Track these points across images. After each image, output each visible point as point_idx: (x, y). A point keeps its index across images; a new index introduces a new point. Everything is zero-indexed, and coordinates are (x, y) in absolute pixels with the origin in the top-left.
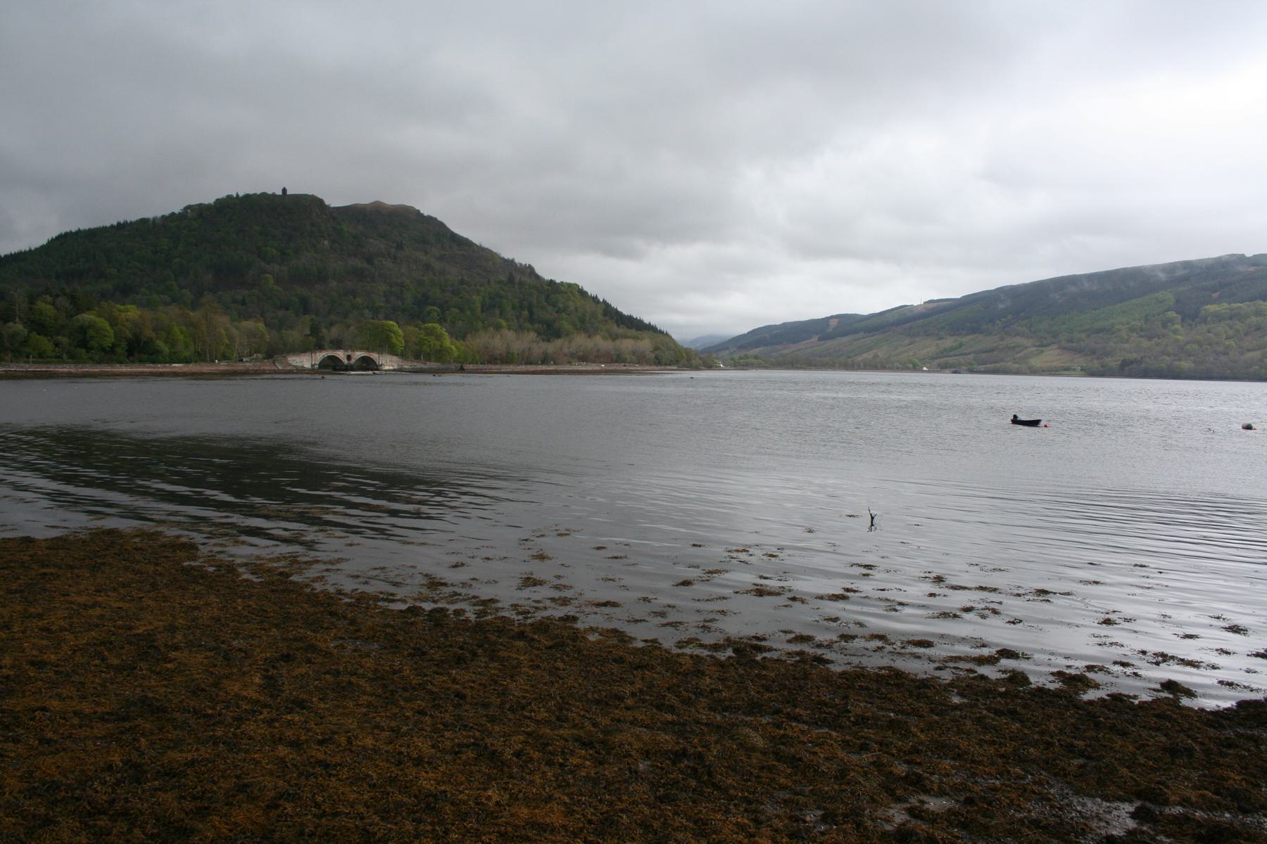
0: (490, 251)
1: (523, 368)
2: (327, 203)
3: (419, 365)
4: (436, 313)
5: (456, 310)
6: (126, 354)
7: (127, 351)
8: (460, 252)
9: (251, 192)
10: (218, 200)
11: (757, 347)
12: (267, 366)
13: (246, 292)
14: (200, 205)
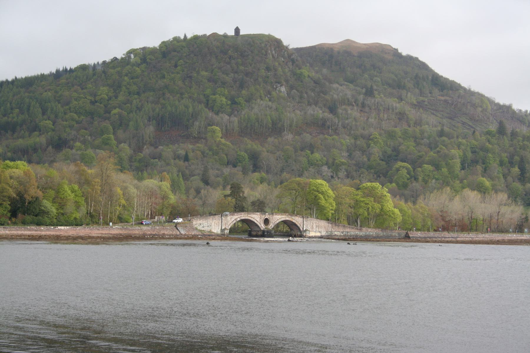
0: (482, 96)
1: (488, 236)
2: (285, 43)
3: (353, 232)
4: (405, 171)
5: (430, 167)
6: (9, 215)
7: (10, 211)
8: (443, 98)
10: (163, 43)
12: (168, 230)
13: (191, 147)
14: (144, 49)
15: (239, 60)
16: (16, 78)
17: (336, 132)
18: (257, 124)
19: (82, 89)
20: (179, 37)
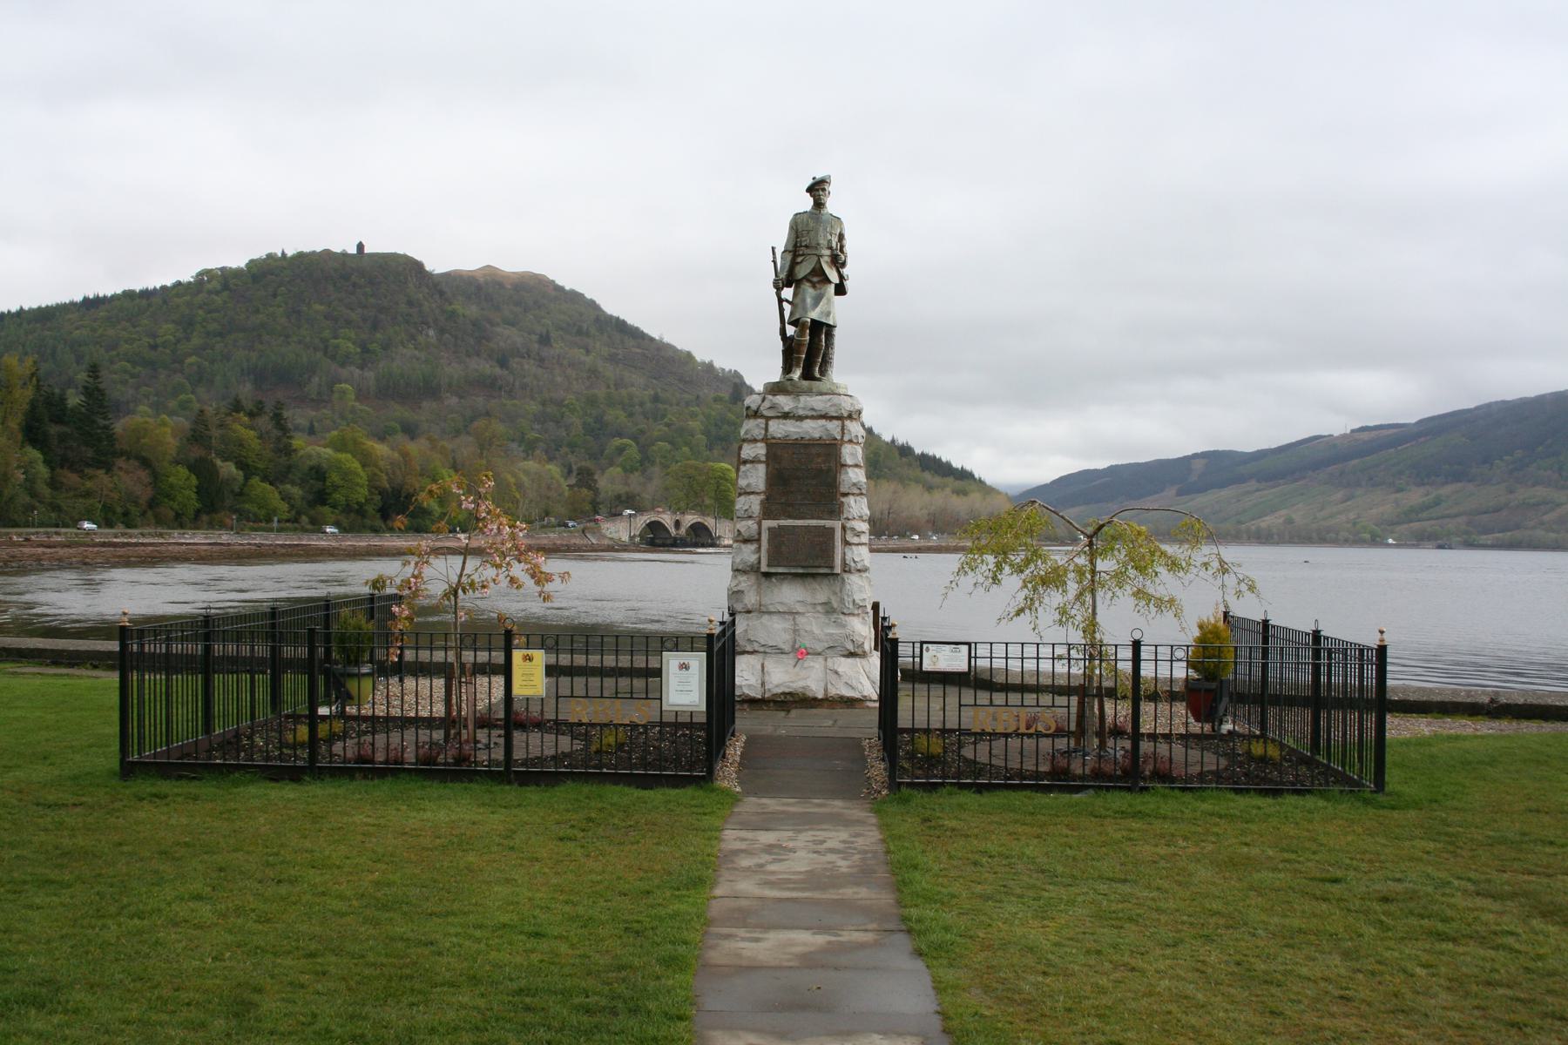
2: (428, 268)
9: (307, 249)
11: (1073, 506)
14: (223, 269)
15: (367, 289)
16: (21, 308)
17: (511, 394)
18: (402, 381)
19: (134, 327)
20: (276, 254)
